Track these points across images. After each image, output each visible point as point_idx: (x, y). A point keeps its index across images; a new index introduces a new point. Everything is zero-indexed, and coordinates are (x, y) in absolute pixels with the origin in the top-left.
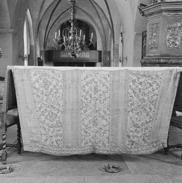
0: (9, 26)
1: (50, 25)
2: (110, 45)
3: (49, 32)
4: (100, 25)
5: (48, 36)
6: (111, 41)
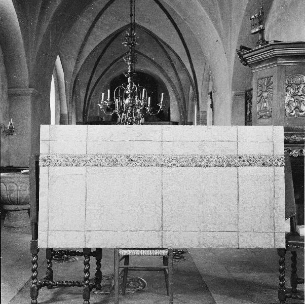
0: (27, 83)
1: (94, 81)
2: (193, 111)
3: (90, 96)
4: (175, 81)
5: (89, 99)
6: (193, 106)
